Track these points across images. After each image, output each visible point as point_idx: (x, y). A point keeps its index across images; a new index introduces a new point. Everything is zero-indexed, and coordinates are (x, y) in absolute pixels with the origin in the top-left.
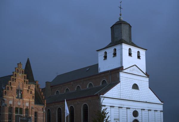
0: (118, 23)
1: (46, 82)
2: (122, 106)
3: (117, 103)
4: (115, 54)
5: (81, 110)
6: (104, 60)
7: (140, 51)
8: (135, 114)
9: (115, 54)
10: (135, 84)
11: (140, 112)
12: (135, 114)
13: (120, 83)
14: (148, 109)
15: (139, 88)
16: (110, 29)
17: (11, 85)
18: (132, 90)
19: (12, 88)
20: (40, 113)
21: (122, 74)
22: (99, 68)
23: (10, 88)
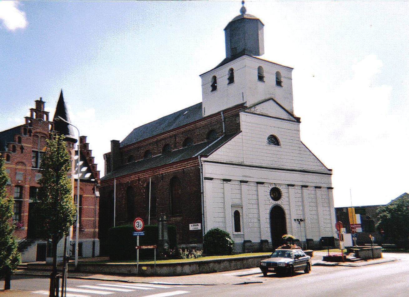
0: (239, 18)
1: (36, 101)
2: (307, 184)
3: (236, 173)
4: (231, 80)
5: (215, 143)
6: (212, 91)
7: (280, 71)
8: (276, 193)
9: (231, 80)
10: (272, 135)
11: (283, 190)
12: (276, 193)
13: (240, 134)
14: (301, 184)
15: (281, 143)
16: (224, 32)
17: (20, 142)
18: (265, 147)
19: (22, 148)
20: (88, 197)
21: (244, 117)
22: (203, 108)
23: (18, 149)
